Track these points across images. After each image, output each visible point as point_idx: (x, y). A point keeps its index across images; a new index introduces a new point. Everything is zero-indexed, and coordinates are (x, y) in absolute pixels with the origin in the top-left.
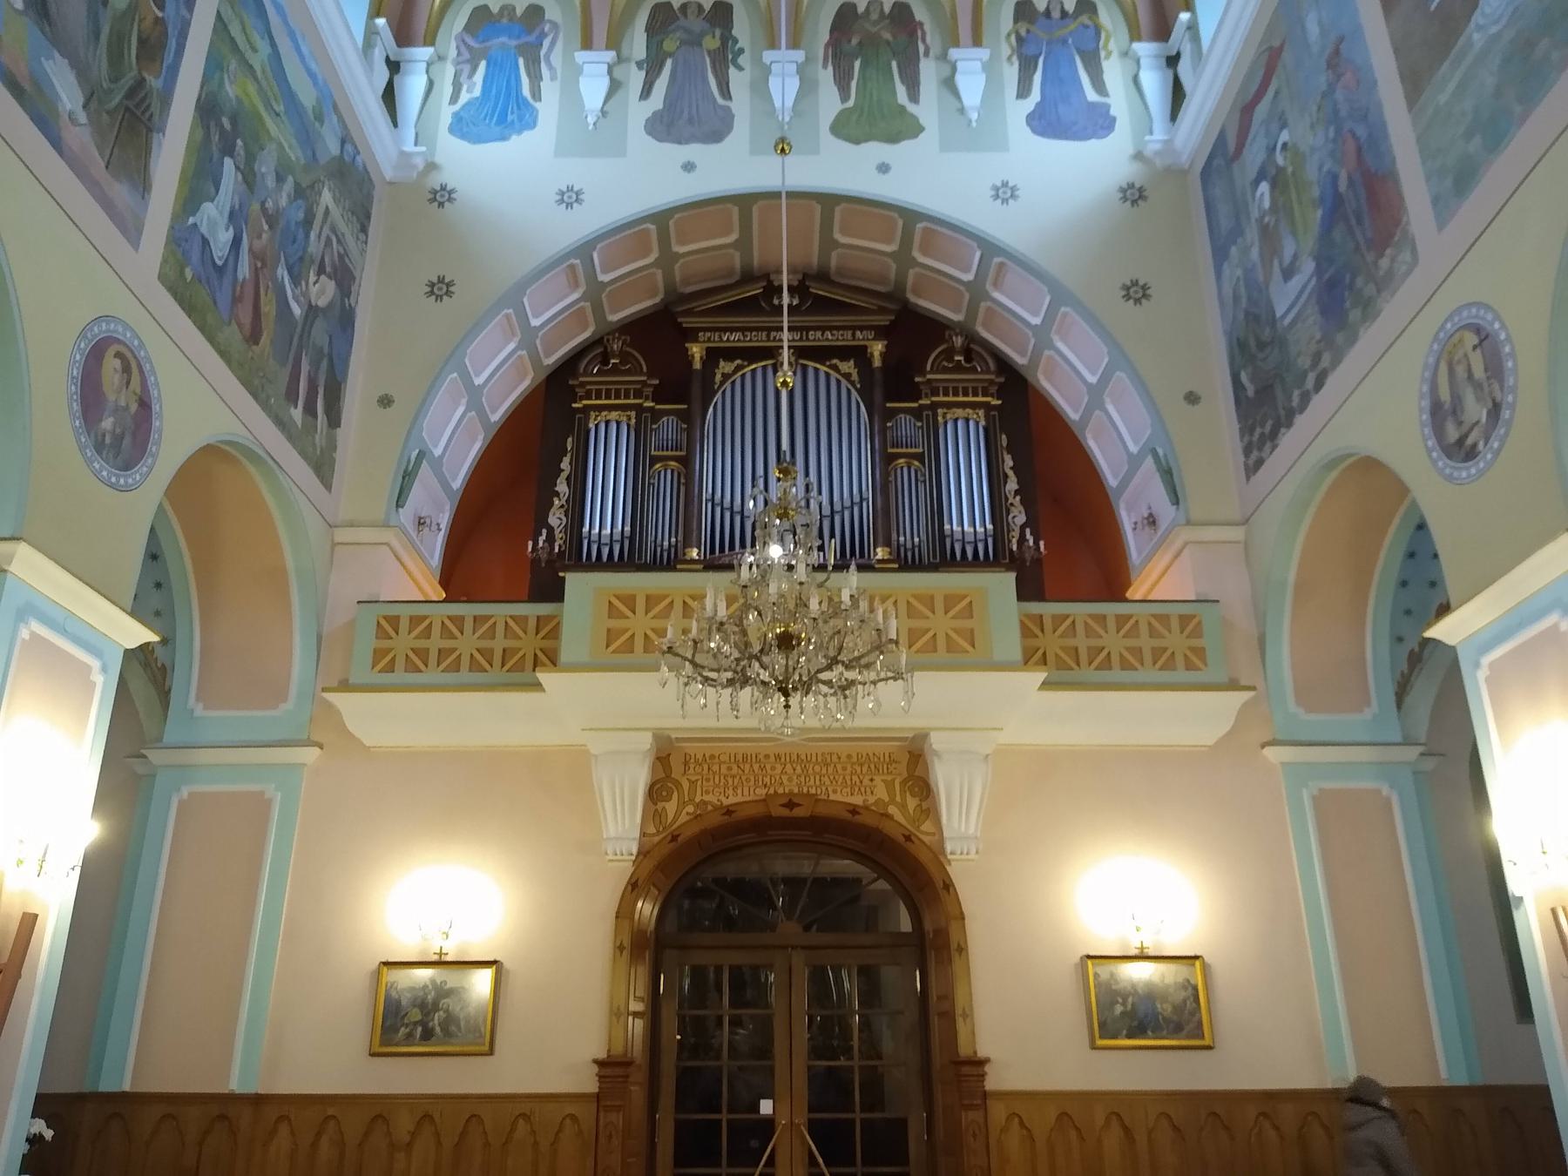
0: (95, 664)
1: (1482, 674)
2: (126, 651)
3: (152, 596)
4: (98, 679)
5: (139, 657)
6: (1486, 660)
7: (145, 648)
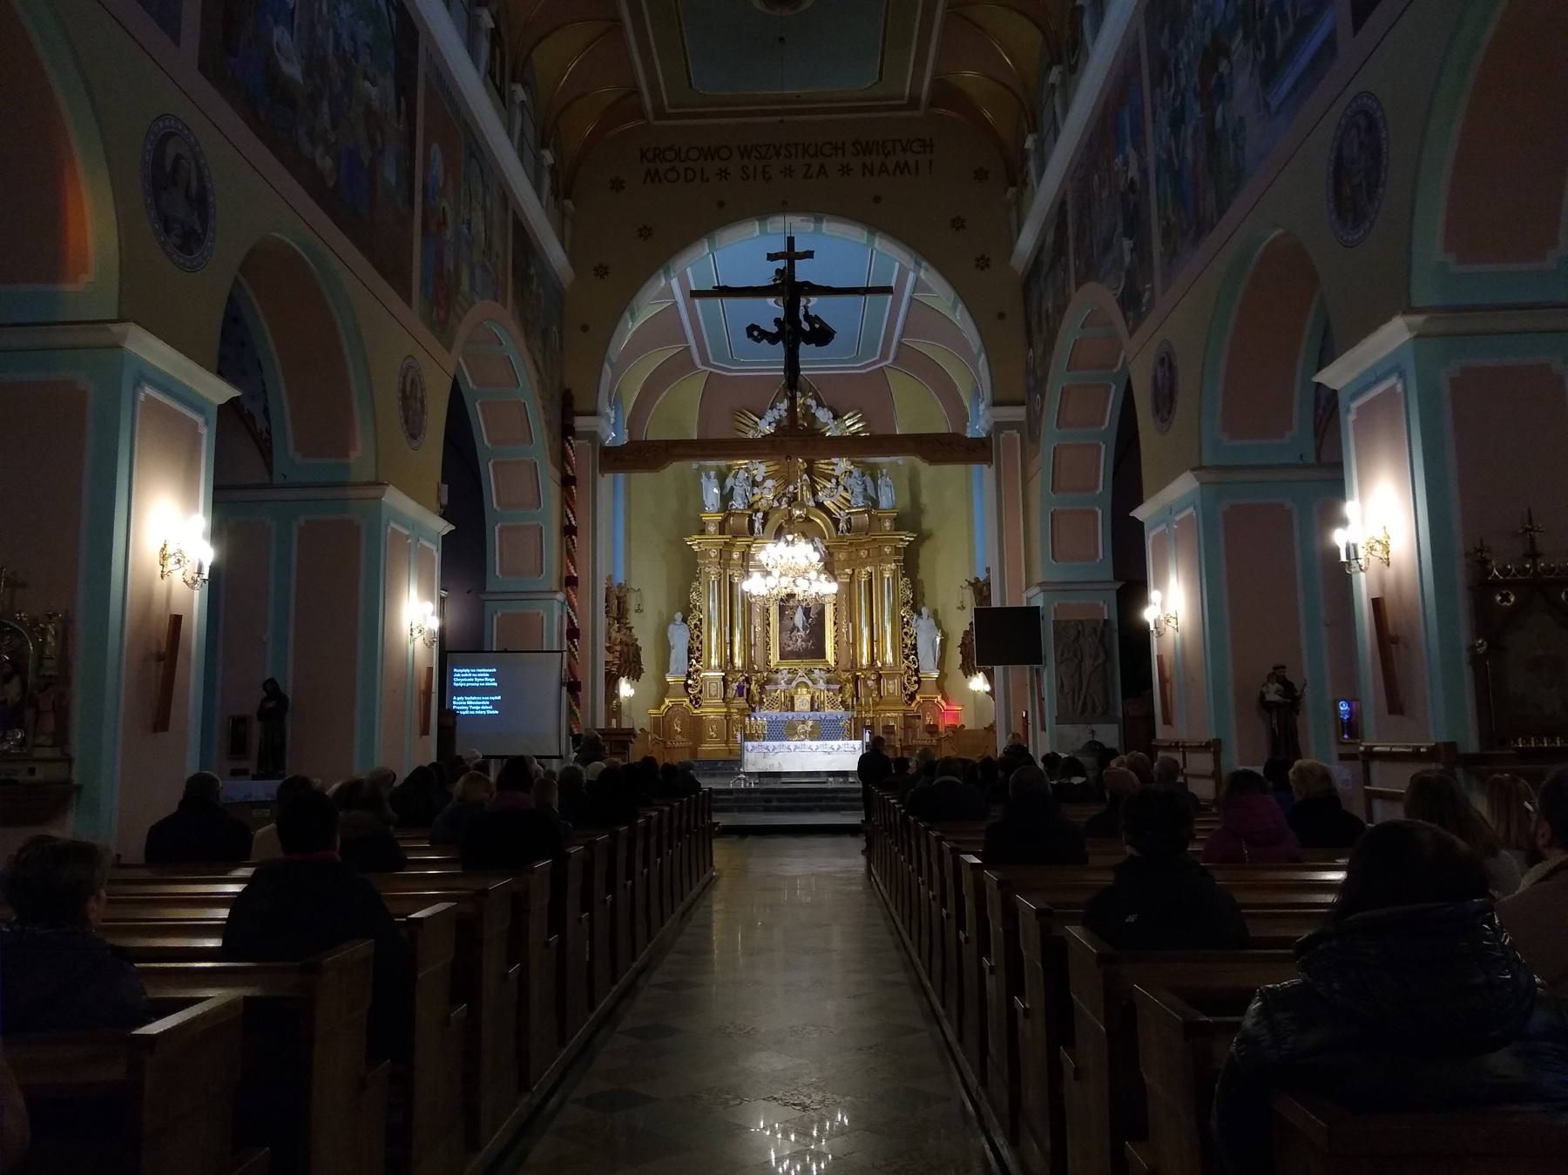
0: (200, 420)
1: (1351, 417)
2: (220, 406)
3: (231, 359)
4: (204, 431)
5: (229, 412)
6: (1354, 405)
7: (233, 402)
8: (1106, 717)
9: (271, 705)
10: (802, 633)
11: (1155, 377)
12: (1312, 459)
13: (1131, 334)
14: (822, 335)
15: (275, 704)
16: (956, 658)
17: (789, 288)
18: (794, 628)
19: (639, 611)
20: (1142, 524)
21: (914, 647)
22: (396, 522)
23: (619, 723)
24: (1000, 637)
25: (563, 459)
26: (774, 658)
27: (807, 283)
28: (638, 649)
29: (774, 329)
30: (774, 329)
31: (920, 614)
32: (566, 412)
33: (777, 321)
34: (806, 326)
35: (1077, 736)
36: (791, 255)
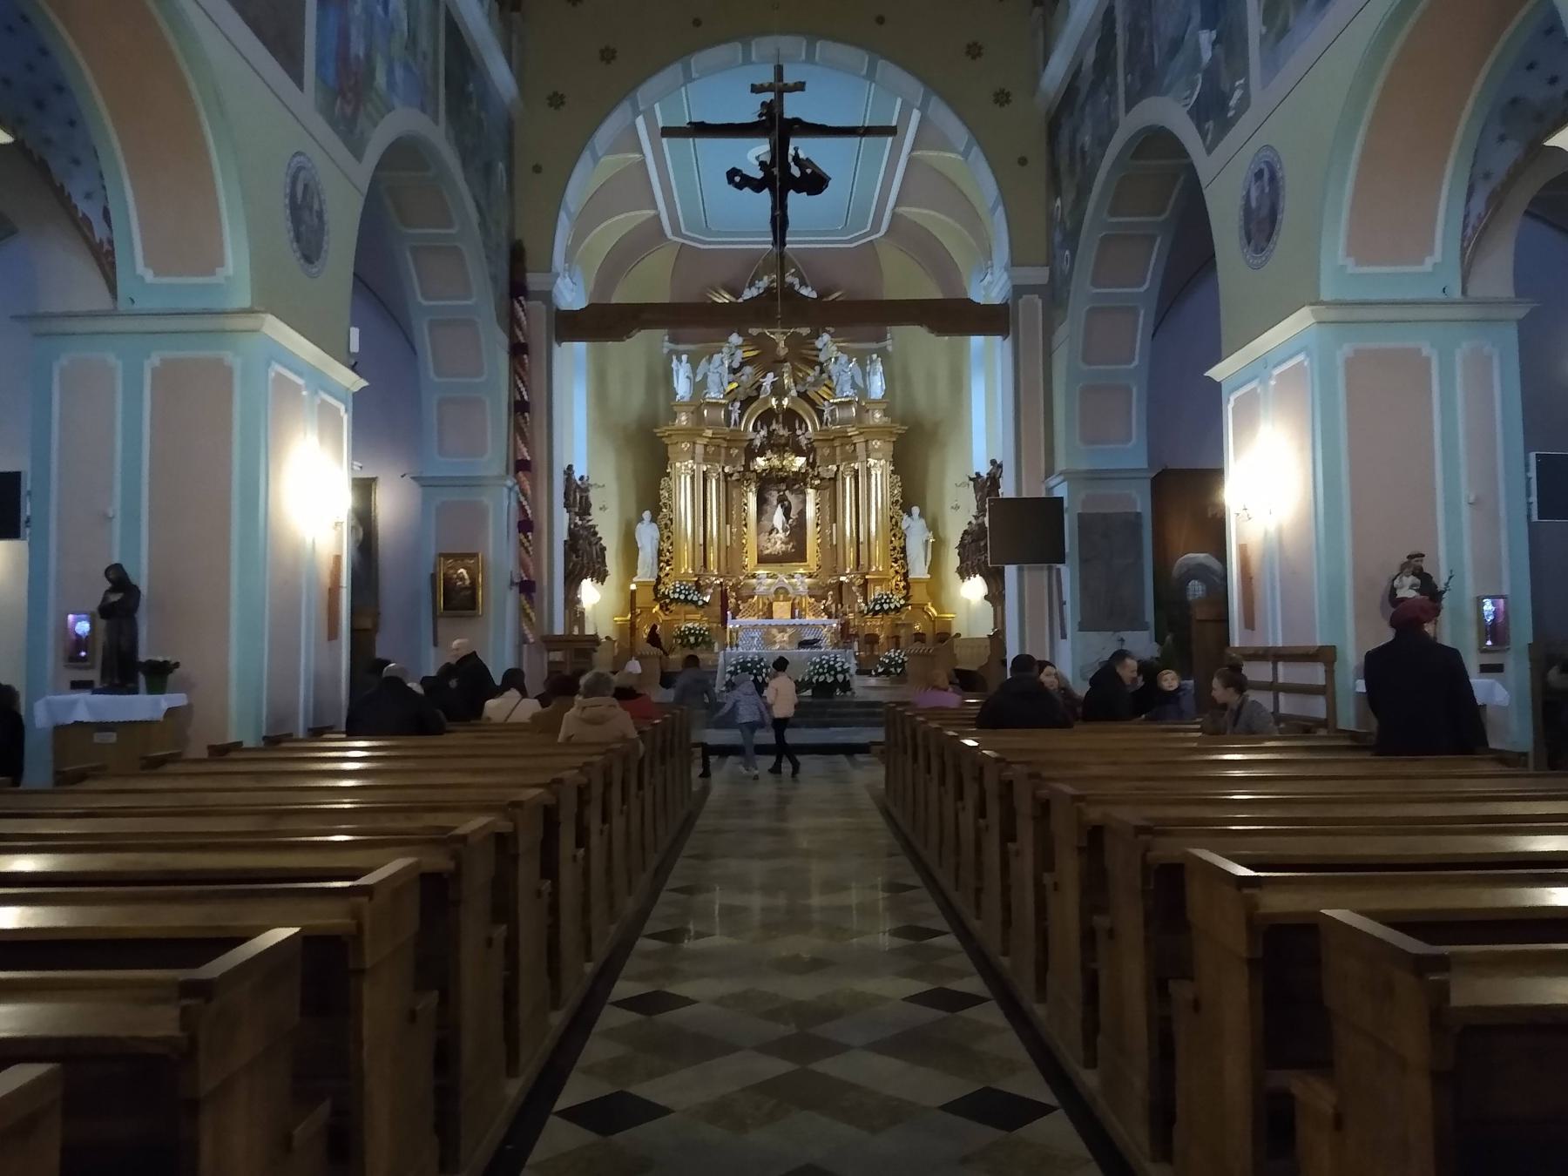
8: (1137, 624)
9: (115, 598)
10: (781, 535)
11: (1247, 198)
12: (1456, 294)
13: (1209, 151)
14: (815, 182)
15: (120, 602)
16: (953, 560)
17: (775, 125)
18: (773, 530)
19: (603, 508)
20: (1219, 385)
21: (904, 550)
22: (280, 363)
23: (582, 628)
24: (1015, 532)
25: (511, 322)
26: (750, 560)
27: (797, 121)
28: (603, 549)
29: (759, 175)
30: (759, 175)
31: (910, 515)
32: (517, 277)
33: (762, 164)
34: (796, 171)
35: (1102, 645)
36: (780, 88)
